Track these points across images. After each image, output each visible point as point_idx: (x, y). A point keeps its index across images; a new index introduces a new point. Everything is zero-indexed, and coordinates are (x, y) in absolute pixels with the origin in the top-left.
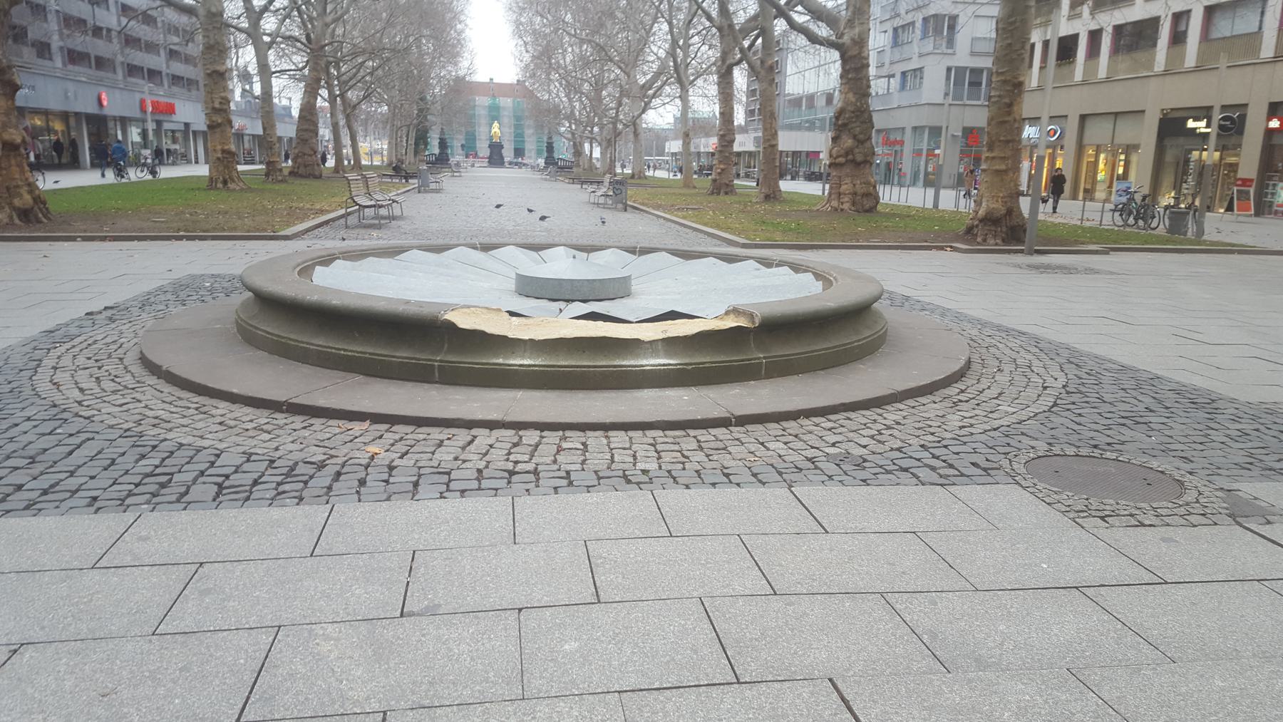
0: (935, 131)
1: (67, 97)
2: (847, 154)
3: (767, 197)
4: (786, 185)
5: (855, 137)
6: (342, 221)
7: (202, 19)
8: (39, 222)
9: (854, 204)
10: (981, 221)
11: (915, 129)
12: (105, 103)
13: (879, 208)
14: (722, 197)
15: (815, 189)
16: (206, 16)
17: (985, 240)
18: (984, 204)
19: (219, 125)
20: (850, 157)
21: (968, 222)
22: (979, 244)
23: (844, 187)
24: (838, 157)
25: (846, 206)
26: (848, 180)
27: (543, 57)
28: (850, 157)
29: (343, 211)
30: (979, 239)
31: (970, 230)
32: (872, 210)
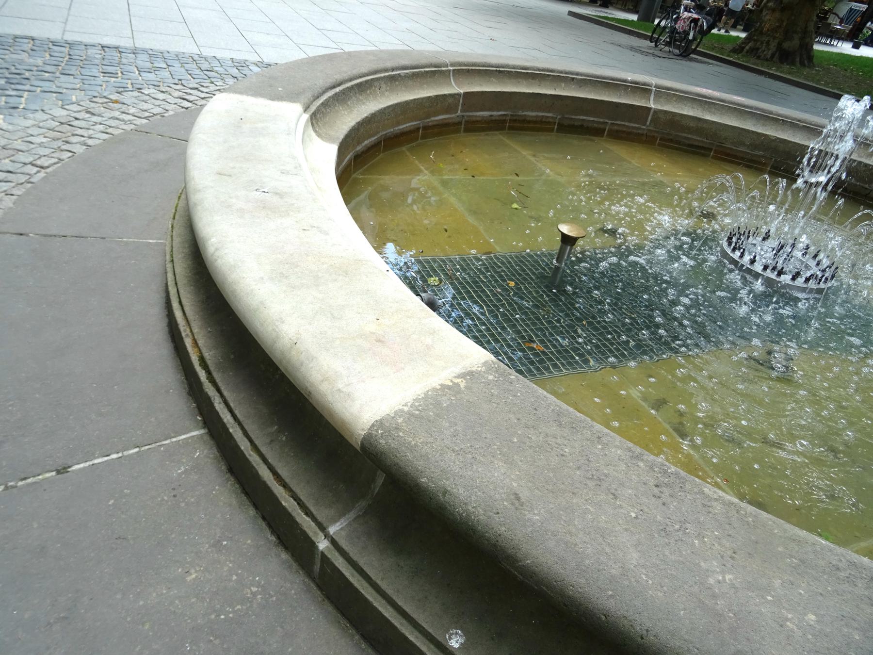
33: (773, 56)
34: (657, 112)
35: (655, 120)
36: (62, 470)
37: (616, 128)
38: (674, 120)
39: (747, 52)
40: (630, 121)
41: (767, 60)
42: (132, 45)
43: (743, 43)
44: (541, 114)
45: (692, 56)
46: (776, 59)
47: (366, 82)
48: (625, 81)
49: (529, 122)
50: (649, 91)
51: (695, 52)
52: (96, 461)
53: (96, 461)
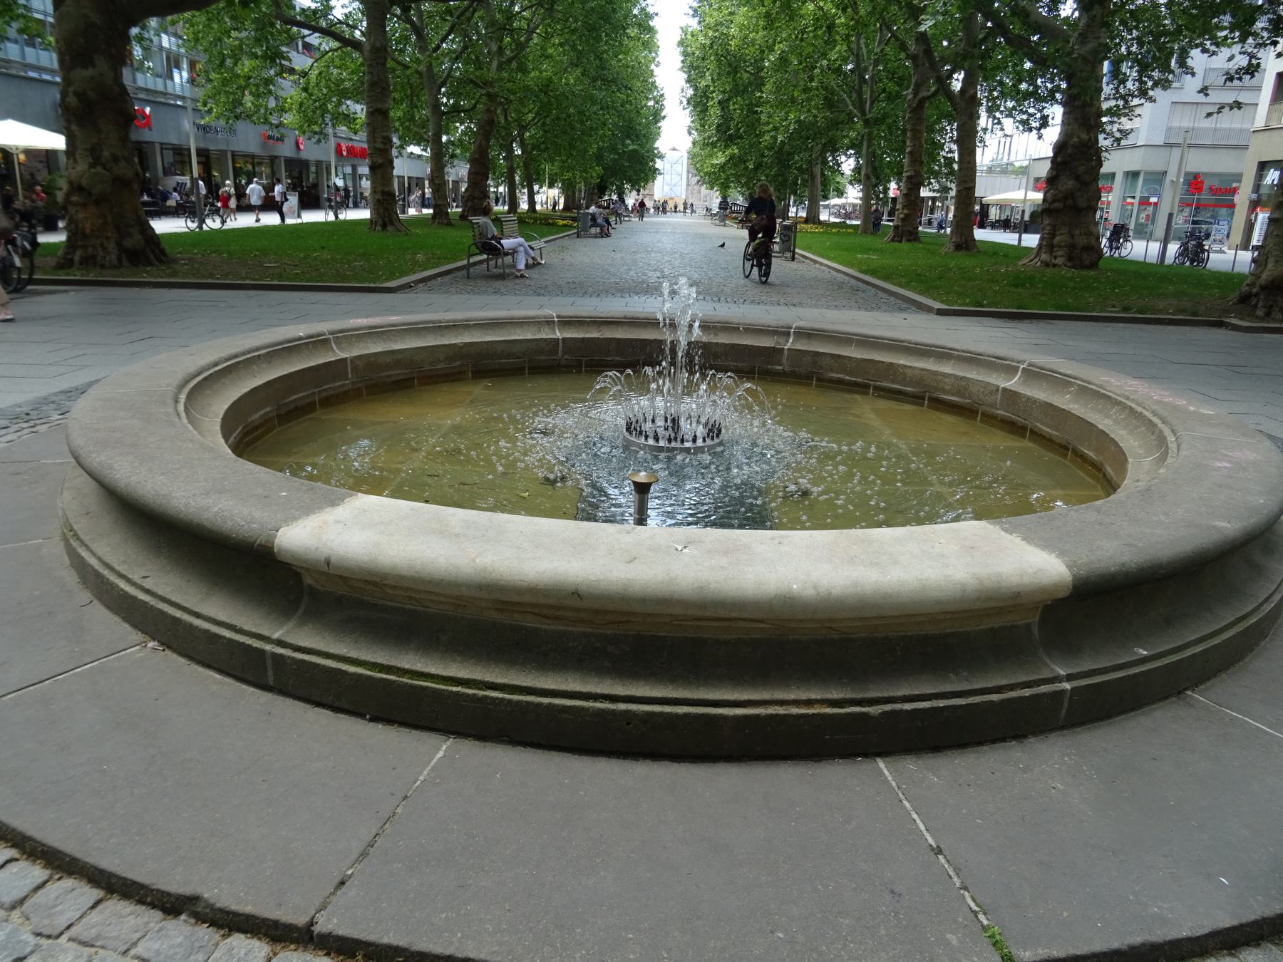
0: (1157, 178)
1: (298, 147)
2: (1066, 198)
3: (958, 247)
4: (980, 234)
5: (1077, 178)
6: (464, 272)
7: (366, 54)
8: (151, 264)
9: (1070, 258)
10: (1263, 288)
11: (1127, 174)
12: (302, 147)
13: (1101, 264)
14: (905, 246)
15: (365, 214)
16: (371, 52)
17: (1268, 315)
18: (1270, 266)
19: (380, 166)
20: (1070, 202)
21: (1245, 289)
22: (1261, 319)
23: (1057, 239)
24: (1053, 202)
25: (1059, 261)
26: (1065, 230)
27: (1061, 554)
28: (1070, 202)
29: (465, 262)
30: (1260, 313)
31: (1244, 299)
32: (1093, 265)
33: (120, 260)
34: (354, 359)
35: (355, 370)
36: (939, 851)
37: (324, 394)
38: (370, 362)
39: (81, 263)
40: (334, 381)
41: (115, 267)
42: (1016, 243)
43: (67, 254)
44: (262, 412)
45: (29, 287)
46: (125, 262)
47: (886, 278)
48: (301, 338)
49: (256, 428)
50: (326, 341)
51: (31, 281)
52: (922, 827)
53: (922, 827)
